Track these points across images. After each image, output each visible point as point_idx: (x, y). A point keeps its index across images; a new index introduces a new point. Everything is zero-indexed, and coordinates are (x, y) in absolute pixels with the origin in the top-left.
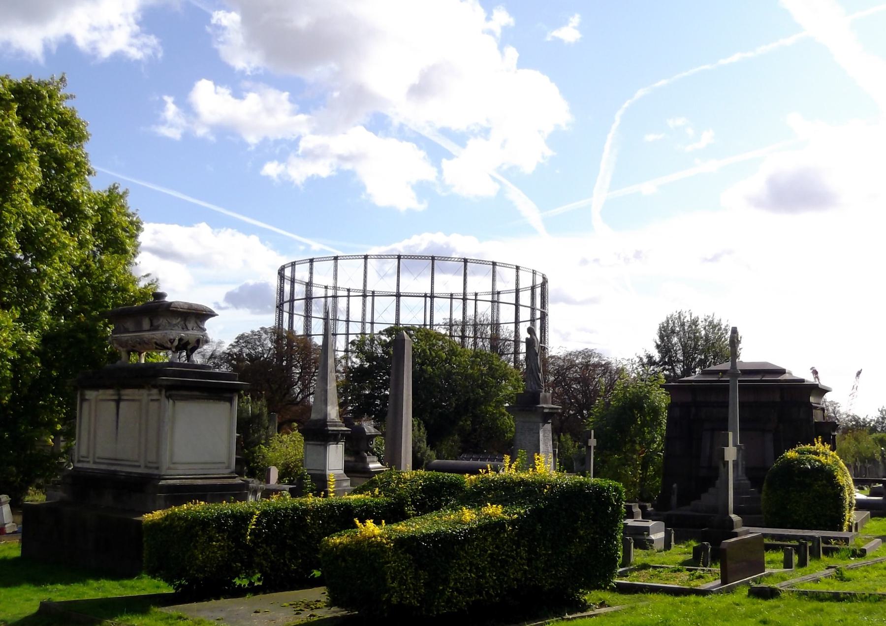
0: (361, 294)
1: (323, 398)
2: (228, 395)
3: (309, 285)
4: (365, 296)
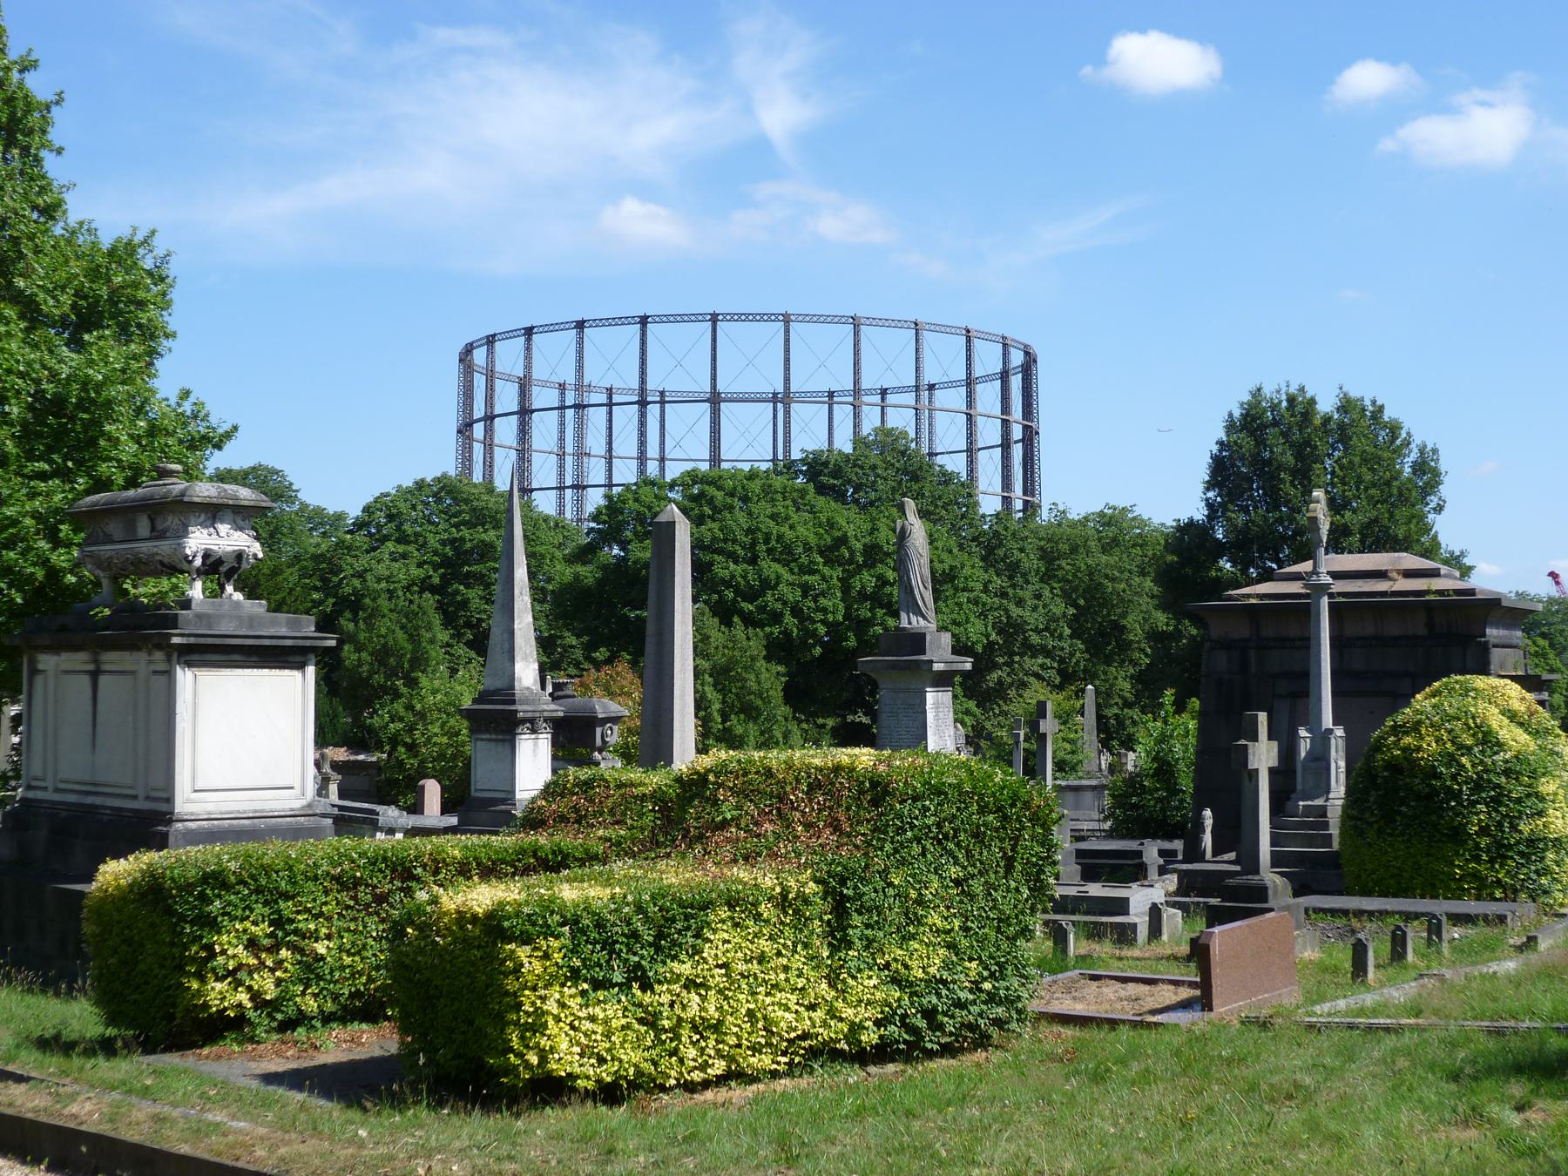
0: (636, 398)
1: (507, 646)
2: (298, 659)
3: (524, 386)
4: (643, 403)
